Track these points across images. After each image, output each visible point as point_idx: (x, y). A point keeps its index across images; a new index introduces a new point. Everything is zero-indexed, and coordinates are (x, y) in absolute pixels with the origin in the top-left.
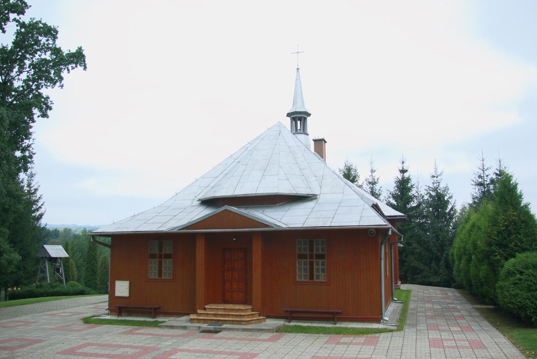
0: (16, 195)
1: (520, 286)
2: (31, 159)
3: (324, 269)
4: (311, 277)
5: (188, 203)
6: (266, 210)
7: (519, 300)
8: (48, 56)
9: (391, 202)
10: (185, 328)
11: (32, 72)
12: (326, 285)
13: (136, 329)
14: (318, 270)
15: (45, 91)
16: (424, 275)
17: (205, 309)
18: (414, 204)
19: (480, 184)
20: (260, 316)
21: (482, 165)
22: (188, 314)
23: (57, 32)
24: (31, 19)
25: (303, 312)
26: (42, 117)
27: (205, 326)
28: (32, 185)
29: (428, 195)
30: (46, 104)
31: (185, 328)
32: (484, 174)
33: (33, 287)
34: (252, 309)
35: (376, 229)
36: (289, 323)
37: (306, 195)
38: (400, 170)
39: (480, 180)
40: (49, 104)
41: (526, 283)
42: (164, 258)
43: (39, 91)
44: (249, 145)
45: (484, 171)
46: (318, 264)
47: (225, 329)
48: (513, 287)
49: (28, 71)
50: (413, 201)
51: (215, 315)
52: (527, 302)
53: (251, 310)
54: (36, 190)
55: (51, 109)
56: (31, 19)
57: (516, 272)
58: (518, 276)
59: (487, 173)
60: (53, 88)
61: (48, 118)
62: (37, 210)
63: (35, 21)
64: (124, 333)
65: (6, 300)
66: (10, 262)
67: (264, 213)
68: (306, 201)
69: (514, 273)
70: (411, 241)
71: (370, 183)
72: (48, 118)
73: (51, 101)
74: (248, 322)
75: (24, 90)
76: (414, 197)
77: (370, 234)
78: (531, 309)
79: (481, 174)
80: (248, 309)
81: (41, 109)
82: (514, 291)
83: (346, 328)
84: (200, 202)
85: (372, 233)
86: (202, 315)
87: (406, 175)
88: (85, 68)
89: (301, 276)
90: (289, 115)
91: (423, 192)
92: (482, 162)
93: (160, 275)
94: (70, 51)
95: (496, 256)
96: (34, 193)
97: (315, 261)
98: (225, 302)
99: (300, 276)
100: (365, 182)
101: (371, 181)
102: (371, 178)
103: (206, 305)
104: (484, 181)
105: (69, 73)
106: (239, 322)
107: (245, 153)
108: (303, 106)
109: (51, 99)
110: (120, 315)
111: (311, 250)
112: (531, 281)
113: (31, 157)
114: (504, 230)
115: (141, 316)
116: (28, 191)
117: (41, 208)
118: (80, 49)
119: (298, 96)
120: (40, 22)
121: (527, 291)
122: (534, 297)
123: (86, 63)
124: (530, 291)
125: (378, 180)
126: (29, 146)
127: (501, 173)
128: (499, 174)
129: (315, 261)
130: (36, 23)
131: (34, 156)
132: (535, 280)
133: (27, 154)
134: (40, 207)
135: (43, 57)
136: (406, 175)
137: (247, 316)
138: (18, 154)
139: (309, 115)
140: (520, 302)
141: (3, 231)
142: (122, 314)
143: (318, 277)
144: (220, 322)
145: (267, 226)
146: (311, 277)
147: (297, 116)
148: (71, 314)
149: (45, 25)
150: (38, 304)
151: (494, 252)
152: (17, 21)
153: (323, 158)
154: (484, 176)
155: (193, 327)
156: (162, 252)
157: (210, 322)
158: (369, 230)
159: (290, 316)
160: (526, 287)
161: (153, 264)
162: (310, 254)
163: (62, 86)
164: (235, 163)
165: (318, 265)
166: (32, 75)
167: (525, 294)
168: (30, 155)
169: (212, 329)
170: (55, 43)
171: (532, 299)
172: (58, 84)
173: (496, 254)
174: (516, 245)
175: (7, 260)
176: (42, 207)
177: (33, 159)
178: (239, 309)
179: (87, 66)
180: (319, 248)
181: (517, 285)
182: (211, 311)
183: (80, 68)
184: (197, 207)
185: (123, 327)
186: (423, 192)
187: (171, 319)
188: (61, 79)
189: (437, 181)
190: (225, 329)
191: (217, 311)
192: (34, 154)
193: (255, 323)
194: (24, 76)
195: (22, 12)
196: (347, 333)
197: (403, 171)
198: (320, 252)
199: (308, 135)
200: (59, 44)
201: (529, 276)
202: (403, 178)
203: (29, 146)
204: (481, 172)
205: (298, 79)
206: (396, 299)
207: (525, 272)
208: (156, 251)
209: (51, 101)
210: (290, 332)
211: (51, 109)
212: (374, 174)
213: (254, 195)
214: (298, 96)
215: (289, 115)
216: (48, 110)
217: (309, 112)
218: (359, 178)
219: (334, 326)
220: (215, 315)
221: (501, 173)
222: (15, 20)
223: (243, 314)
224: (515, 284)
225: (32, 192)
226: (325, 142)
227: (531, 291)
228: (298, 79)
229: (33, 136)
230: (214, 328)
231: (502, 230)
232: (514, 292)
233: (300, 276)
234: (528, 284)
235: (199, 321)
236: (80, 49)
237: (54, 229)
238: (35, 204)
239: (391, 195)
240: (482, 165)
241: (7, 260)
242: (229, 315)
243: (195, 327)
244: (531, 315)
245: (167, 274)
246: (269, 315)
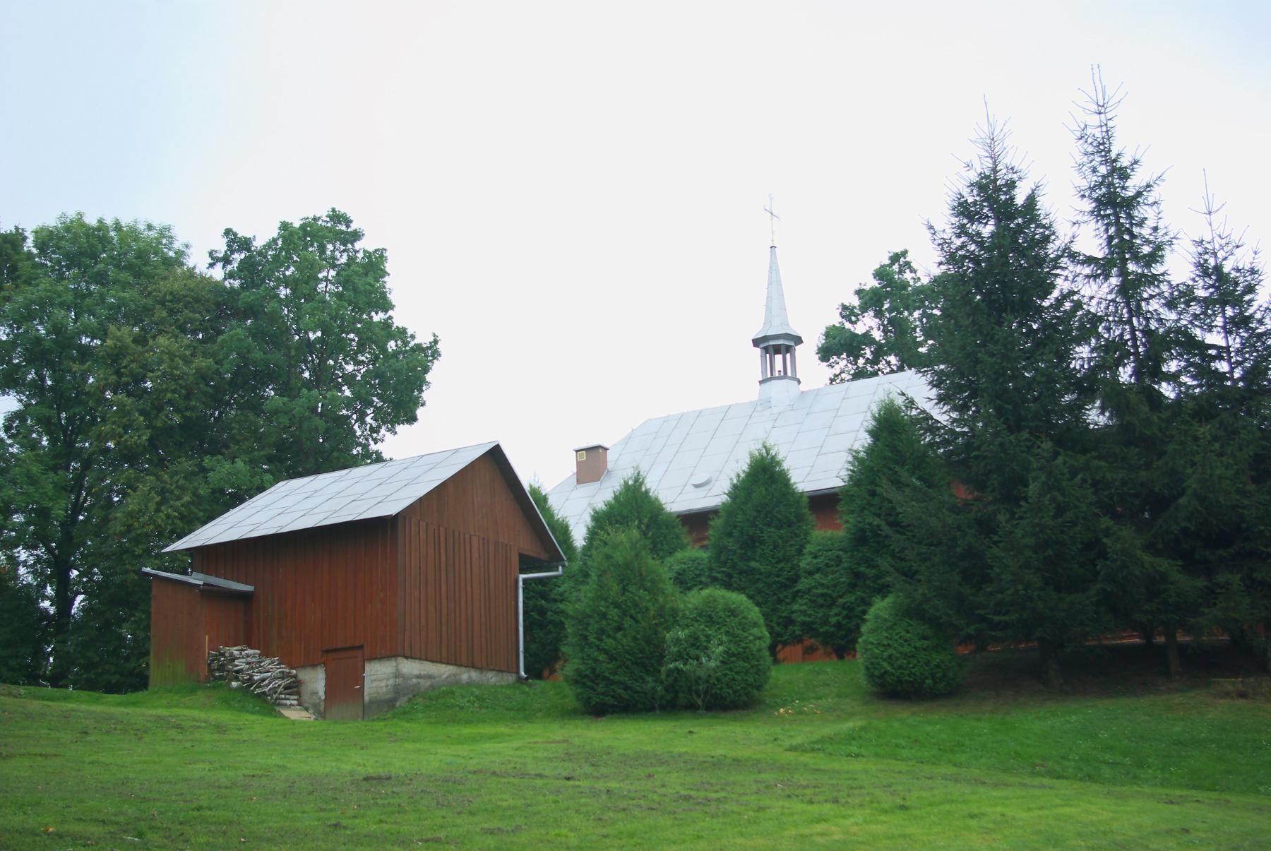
90: (756, 342)
205: (773, 269)
215: (756, 342)
228: (773, 269)
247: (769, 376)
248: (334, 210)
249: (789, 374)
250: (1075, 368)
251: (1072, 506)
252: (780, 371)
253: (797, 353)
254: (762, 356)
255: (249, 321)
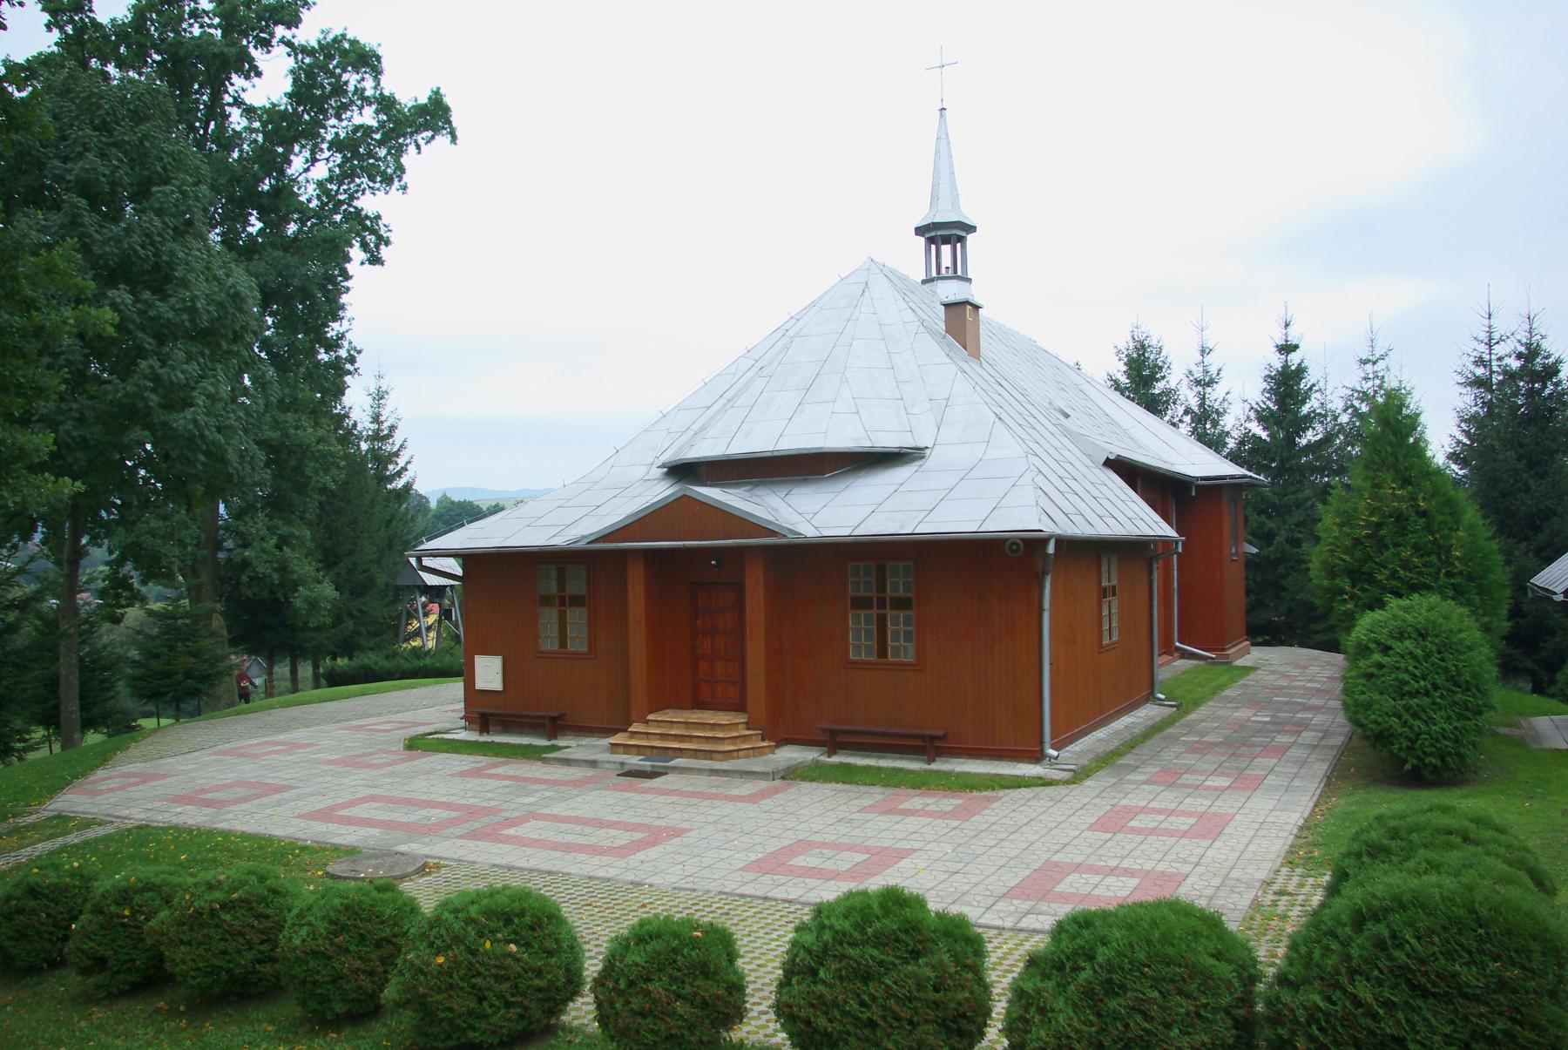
0: (318, 451)
1: (1378, 682)
2: (352, 365)
3: (911, 632)
4: (882, 652)
5: (640, 472)
6: (795, 491)
7: (1373, 717)
8: (368, 117)
9: (1253, 431)
10: (593, 764)
11: (338, 158)
12: (915, 670)
13: (495, 766)
14: (896, 634)
15: (368, 203)
16: (1331, 623)
17: (647, 722)
18: (1310, 436)
19: (1478, 383)
20: (763, 740)
21: (1487, 329)
22: (614, 732)
23: (379, 58)
24: (323, 32)
25: (859, 733)
26: (370, 263)
27: (634, 761)
28: (382, 419)
29: (1350, 411)
30: (374, 232)
31: (593, 764)
32: (1490, 354)
33: (371, 659)
34: (746, 723)
35: (1025, 540)
36: (829, 757)
37: (897, 450)
38: (1277, 346)
39: (1480, 371)
40: (382, 232)
41: (1393, 676)
42: (570, 606)
43: (356, 203)
44: (794, 321)
45: (1490, 346)
46: (896, 622)
47: (674, 769)
48: (1364, 685)
49: (327, 159)
50: (1314, 429)
51: (663, 736)
52: (1391, 723)
53: (744, 726)
54: (393, 428)
55: (387, 243)
56: (323, 32)
57: (1372, 646)
58: (1377, 657)
59: (1500, 350)
60: (387, 193)
61: (382, 264)
62: (399, 474)
63: (330, 37)
64: (462, 774)
65: (317, 686)
66: (313, 605)
67: (790, 499)
68: (897, 466)
69: (1368, 648)
70: (1300, 536)
71: (1198, 383)
72: (382, 264)
73: (385, 226)
74: (728, 755)
75: (324, 205)
76: (1314, 417)
77: (1011, 549)
78: (1402, 740)
79: (1484, 355)
80: (738, 724)
81: (365, 246)
82: (1364, 693)
83: (948, 774)
84: (665, 470)
85: (1015, 547)
86: (637, 736)
87: (1294, 359)
88: (454, 139)
89: (860, 647)
90: (919, 231)
91: (1337, 405)
92: (1486, 322)
93: (563, 643)
94: (416, 101)
95: (1345, 601)
96: (389, 436)
97: (889, 613)
98: (699, 705)
99: (858, 649)
100: (1185, 382)
101: (1198, 375)
102: (1201, 369)
103: (651, 712)
104: (1491, 375)
105: (419, 153)
106: (709, 755)
107: (780, 344)
108: (955, 204)
109: (385, 220)
110: (484, 729)
111: (881, 587)
112: (1407, 671)
113: (352, 360)
114: (1368, 537)
115: (528, 734)
116: (373, 431)
117: (407, 470)
118: (437, 93)
119: (943, 178)
120: (343, 36)
121: (1394, 695)
122: (1411, 711)
123: (454, 124)
124: (1402, 696)
125: (1218, 374)
126: (341, 336)
127: (1531, 353)
128: (1526, 352)
129: (889, 613)
130: (335, 40)
131: (359, 358)
132: (1416, 667)
133: (343, 353)
134: (404, 469)
135: (357, 120)
136: (1294, 359)
137: (729, 741)
138: (323, 356)
139: (971, 229)
140: (1375, 722)
141: (297, 533)
142: (491, 728)
143: (896, 650)
144: (670, 752)
145: (773, 533)
146: (882, 652)
147: (939, 233)
148: (399, 725)
149: (354, 42)
150: (398, 693)
151: (1342, 592)
152: (289, 44)
153: (965, 348)
154: (1490, 360)
155: (609, 762)
156: (564, 590)
157: (649, 752)
158: (1008, 543)
159: (833, 742)
160: (1392, 685)
161: (549, 619)
162: (878, 598)
163: (404, 188)
164: (754, 370)
165: (898, 623)
166: (339, 166)
167: (1388, 703)
168: (350, 355)
169: (649, 769)
170: (379, 85)
171: (1407, 717)
172: (396, 184)
173: (1345, 597)
174: (1393, 575)
175: (306, 600)
176: (409, 467)
177: (356, 365)
178: (715, 725)
179: (457, 133)
180: (899, 583)
181: (1373, 680)
182: (658, 727)
183: (442, 140)
184: (655, 482)
185: (472, 758)
186: (1337, 405)
187: (586, 741)
188: (401, 169)
189: (1375, 372)
190: (674, 769)
191: (671, 728)
192: (359, 352)
193: (747, 757)
194: (320, 171)
195: (293, 22)
196: (939, 786)
197: (1287, 348)
198: (901, 593)
199: (969, 280)
200: (389, 85)
201: (1402, 656)
202: (1286, 366)
203: (341, 336)
204: (1483, 348)
205: (943, 138)
206: (1162, 696)
207: (1394, 646)
208: (553, 588)
209: (385, 226)
210: (812, 780)
211: (387, 243)
212: (1208, 359)
213: (769, 454)
214: (943, 178)
215: (919, 231)
216: (383, 247)
217: (970, 220)
218: (1169, 371)
219: (926, 766)
220: (663, 736)
221: (1531, 353)
222: (283, 41)
223: (720, 735)
224: (1370, 676)
225: (386, 432)
226: (976, 307)
227: (1405, 695)
228: (943, 138)
229: (348, 314)
230: (652, 766)
231: (1364, 537)
232: (1364, 696)
233: (858, 649)
234: (1396, 679)
235: (627, 748)
236: (437, 93)
237: (493, 504)
238: (391, 462)
239: (1252, 415)
240: (1487, 329)
241: (306, 600)
242: (690, 738)
243: (614, 763)
244: (1403, 755)
245: (578, 642)
246: (792, 736)
247: (934, 274)
248: (439, 89)
249: (959, 273)
250: (1495, 983)
251: (1406, 635)
252: (947, 268)
253: (968, 243)
254: (928, 251)
255: (266, 188)
